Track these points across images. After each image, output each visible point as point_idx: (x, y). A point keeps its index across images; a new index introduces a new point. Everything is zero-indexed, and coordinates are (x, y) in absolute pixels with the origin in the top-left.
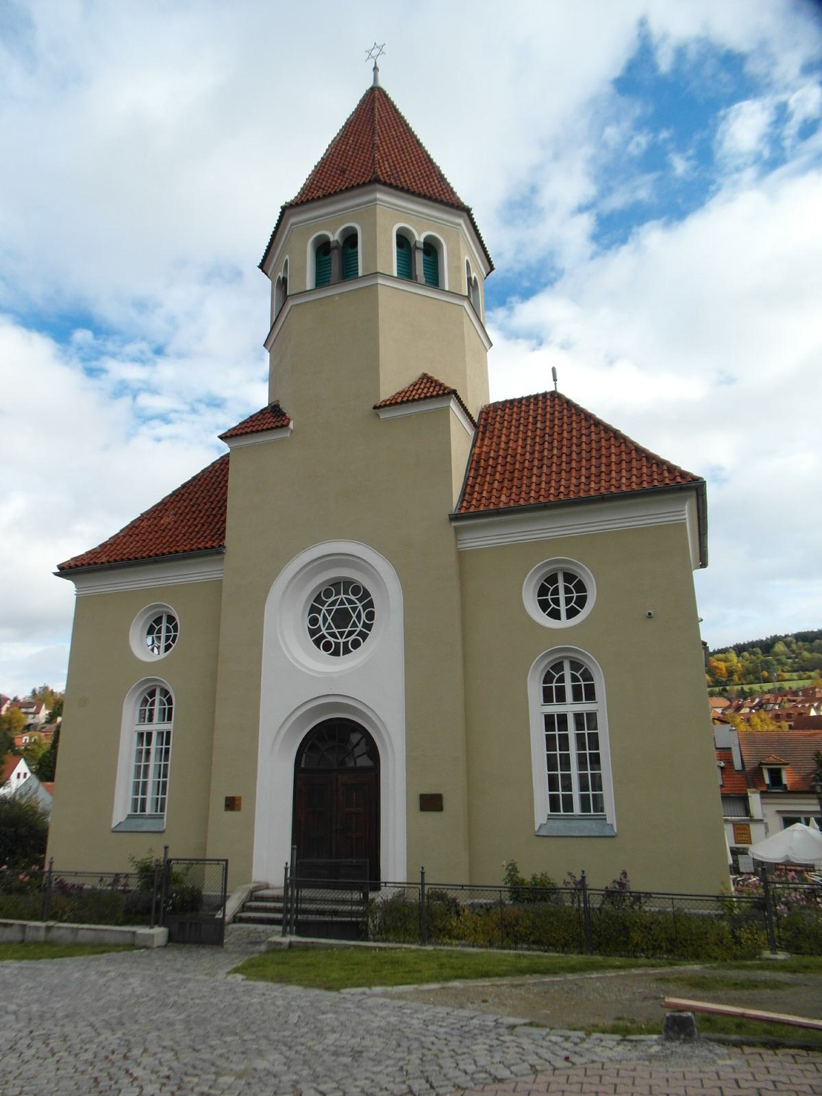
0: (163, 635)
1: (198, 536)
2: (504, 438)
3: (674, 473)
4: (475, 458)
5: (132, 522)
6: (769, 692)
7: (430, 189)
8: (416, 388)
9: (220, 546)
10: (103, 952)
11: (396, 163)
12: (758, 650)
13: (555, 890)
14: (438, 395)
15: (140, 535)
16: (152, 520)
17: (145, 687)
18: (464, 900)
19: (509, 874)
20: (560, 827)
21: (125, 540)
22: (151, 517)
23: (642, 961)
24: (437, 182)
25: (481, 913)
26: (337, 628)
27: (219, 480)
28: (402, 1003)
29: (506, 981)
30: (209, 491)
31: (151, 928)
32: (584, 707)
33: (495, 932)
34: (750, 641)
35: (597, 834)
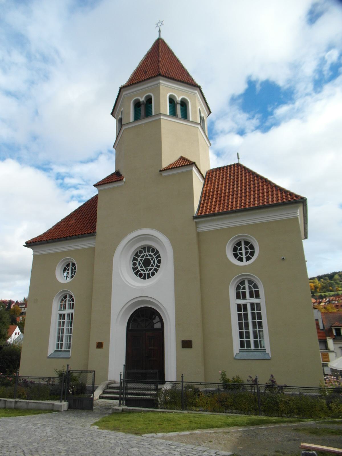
0: (70, 271)
1: (85, 228)
2: (216, 183)
3: (292, 196)
4: (204, 192)
5: (57, 223)
6: (333, 296)
7: (183, 78)
8: (178, 162)
9: (94, 232)
10: (38, 413)
11: (168, 68)
12: (327, 278)
13: (243, 385)
14: (187, 165)
15: (61, 229)
16: (66, 222)
17: (63, 294)
18: (202, 388)
19: (222, 377)
20: (245, 355)
21: (54, 231)
22: (65, 221)
23: (286, 419)
24: (186, 75)
25: (209, 395)
26: (145, 267)
27: (94, 205)
28: (171, 442)
29: (221, 430)
30: (90, 209)
31: (61, 402)
32: (255, 301)
33: (216, 404)
34: (324, 274)
35: (262, 358)
